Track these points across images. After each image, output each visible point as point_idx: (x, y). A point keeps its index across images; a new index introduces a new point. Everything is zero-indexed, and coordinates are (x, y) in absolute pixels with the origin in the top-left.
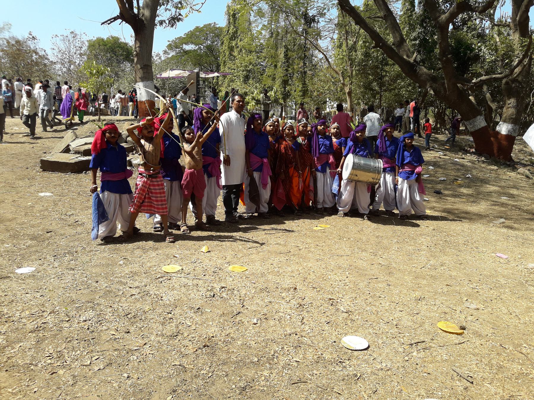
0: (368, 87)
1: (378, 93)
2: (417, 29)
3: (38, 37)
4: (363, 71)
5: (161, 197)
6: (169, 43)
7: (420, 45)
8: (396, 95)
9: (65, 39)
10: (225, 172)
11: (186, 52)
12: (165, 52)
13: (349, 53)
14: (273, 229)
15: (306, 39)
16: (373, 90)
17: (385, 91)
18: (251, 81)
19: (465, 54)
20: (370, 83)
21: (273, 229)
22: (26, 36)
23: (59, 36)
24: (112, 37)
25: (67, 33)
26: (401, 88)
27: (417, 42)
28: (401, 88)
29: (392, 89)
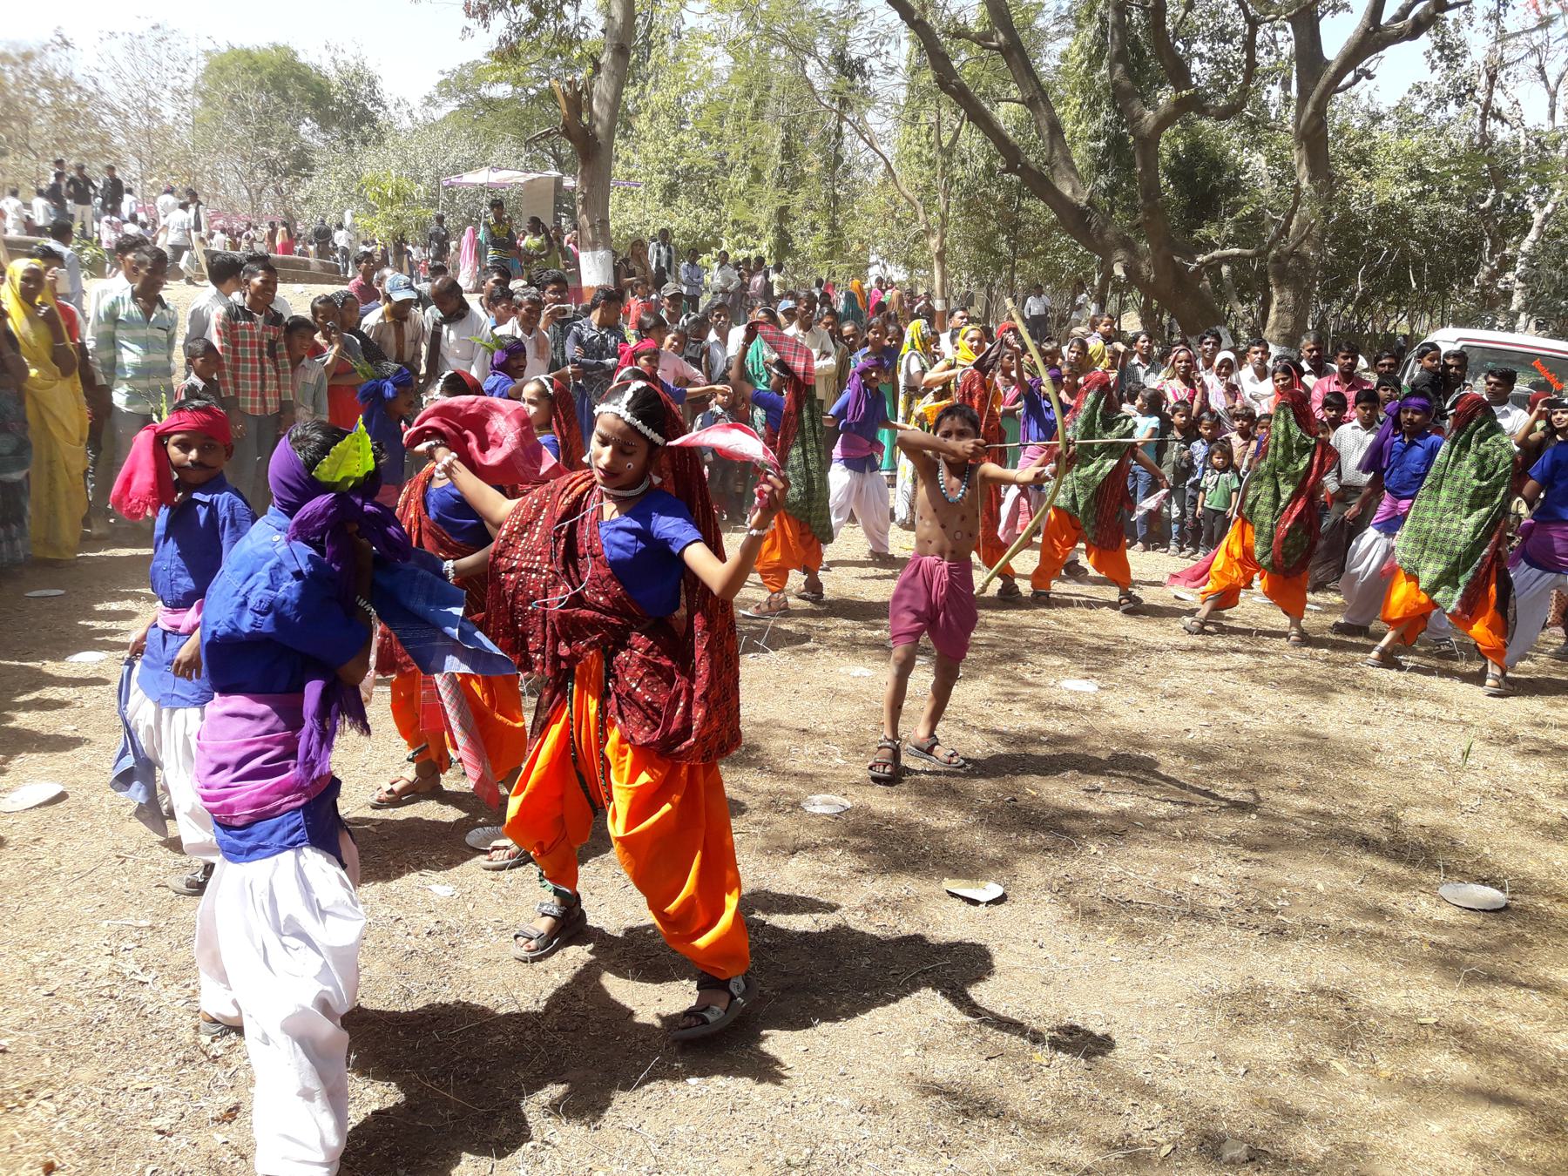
0: (985, 245)
1: (1006, 261)
2: (1103, 114)
3: (77, 43)
4: (973, 205)
5: (1275, 448)
6: (442, 78)
7: (1107, 152)
8: (1047, 266)
9: (135, 43)
10: (645, 437)
11: (491, 104)
12: (430, 101)
13: (1438, 868)
14: (545, 638)
15: (841, 118)
16: (998, 254)
17: (1025, 256)
18: (682, 201)
19: (1207, 179)
20: (993, 236)
21: (545, 638)
22: (47, 36)
23: (118, 34)
24: (277, 48)
25: (143, 27)
26: (1060, 249)
27: (1102, 144)
28: (1060, 249)
29: (1040, 253)
